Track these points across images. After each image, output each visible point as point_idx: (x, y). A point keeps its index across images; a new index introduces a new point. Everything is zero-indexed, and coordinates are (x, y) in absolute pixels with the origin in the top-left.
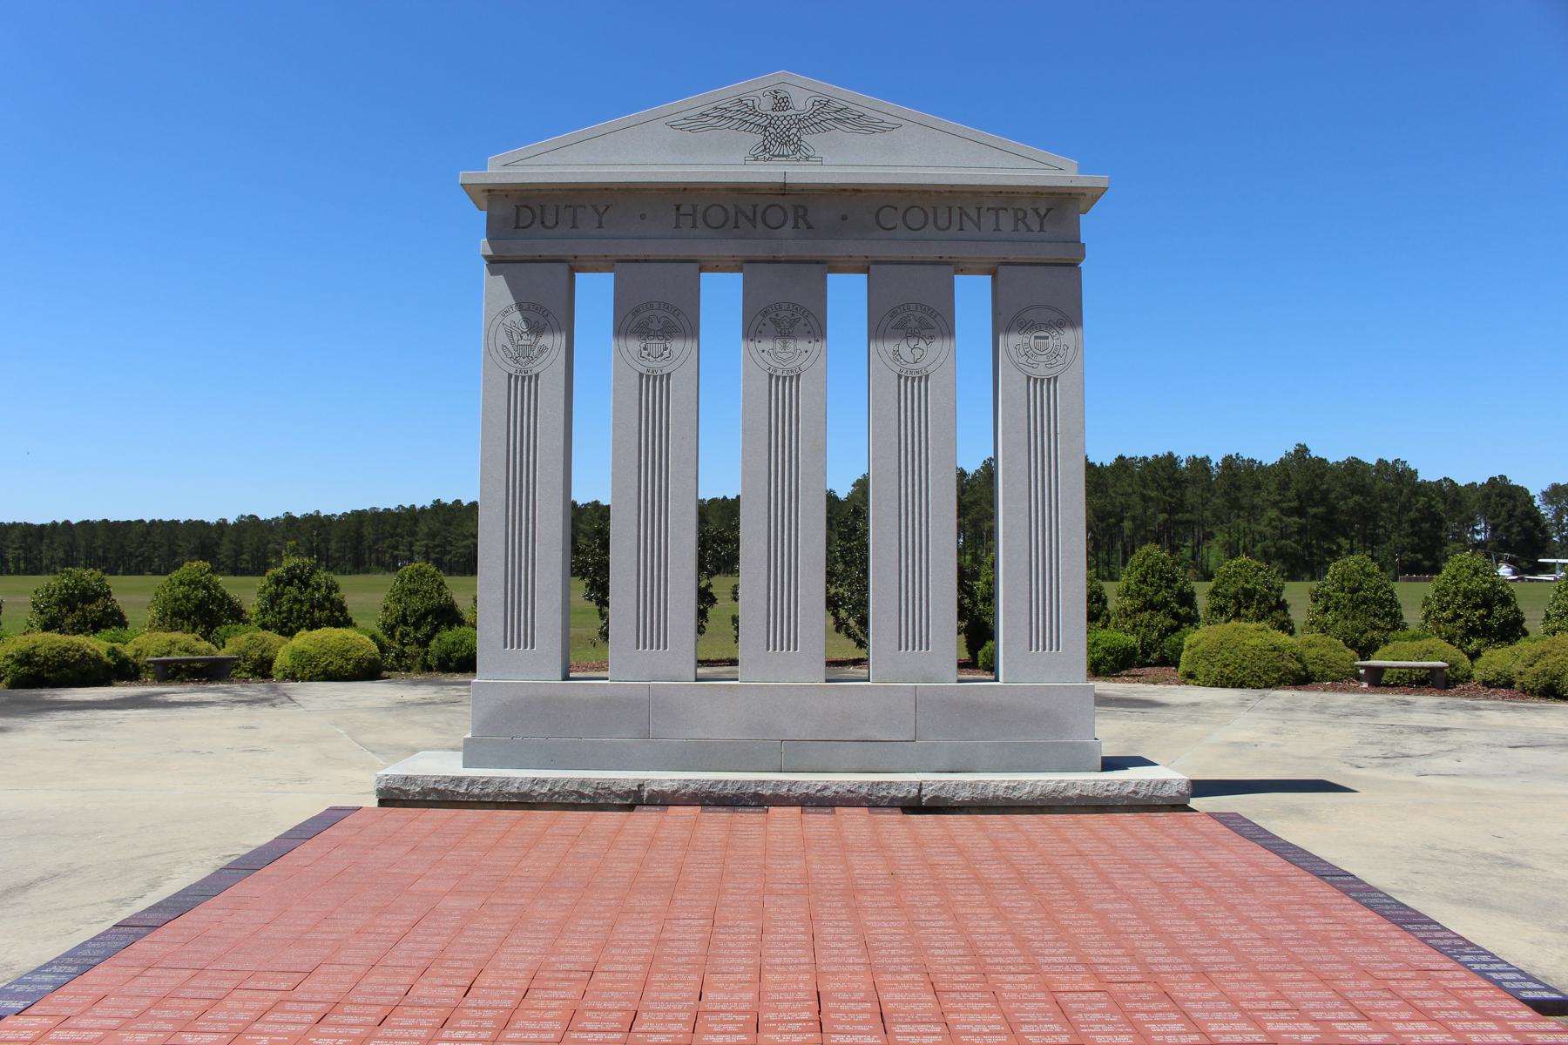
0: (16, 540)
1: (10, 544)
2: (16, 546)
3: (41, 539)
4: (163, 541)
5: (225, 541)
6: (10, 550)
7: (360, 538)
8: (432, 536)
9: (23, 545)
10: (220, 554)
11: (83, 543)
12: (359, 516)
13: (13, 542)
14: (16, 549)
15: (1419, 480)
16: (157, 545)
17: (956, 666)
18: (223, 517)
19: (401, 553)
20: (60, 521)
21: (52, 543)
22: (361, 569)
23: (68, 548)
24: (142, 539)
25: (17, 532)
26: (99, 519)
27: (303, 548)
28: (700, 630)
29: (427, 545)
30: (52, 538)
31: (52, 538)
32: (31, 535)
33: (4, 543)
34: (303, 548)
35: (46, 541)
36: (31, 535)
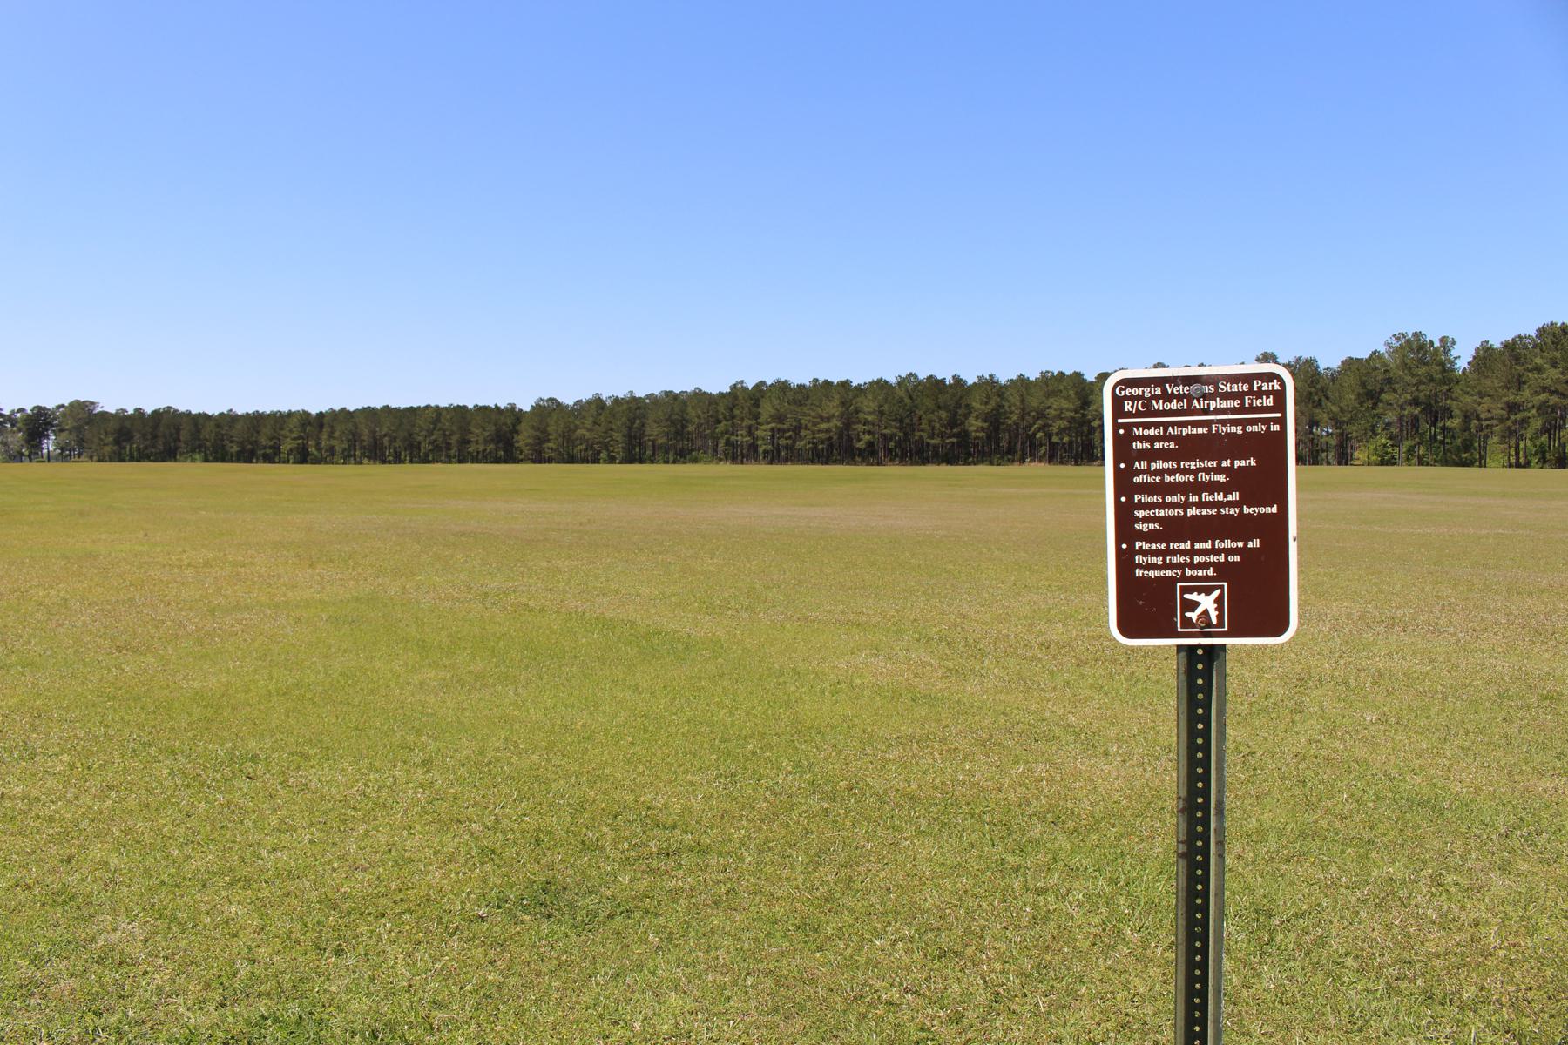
0: (295, 429)
1: (288, 433)
2: (295, 435)
3: (321, 426)
4: (454, 428)
5: (523, 427)
6: (288, 440)
7: (684, 422)
8: (780, 418)
9: (302, 434)
10: (518, 442)
11: (366, 432)
12: (369, 412)
13: (291, 431)
14: (295, 439)
15: (750, 388)
16: (447, 433)
17: (1343, 468)
18: (512, 402)
19: (739, 438)
20: (337, 408)
21: (333, 432)
22: (688, 457)
23: (350, 437)
24: (432, 426)
25: (296, 420)
26: (690, 389)
27: (620, 434)
28: (1168, 367)
29: (772, 430)
30: (332, 427)
31: (332, 427)
32: (310, 424)
33: (283, 432)
34: (620, 434)
35: (326, 430)
36: (310, 424)
